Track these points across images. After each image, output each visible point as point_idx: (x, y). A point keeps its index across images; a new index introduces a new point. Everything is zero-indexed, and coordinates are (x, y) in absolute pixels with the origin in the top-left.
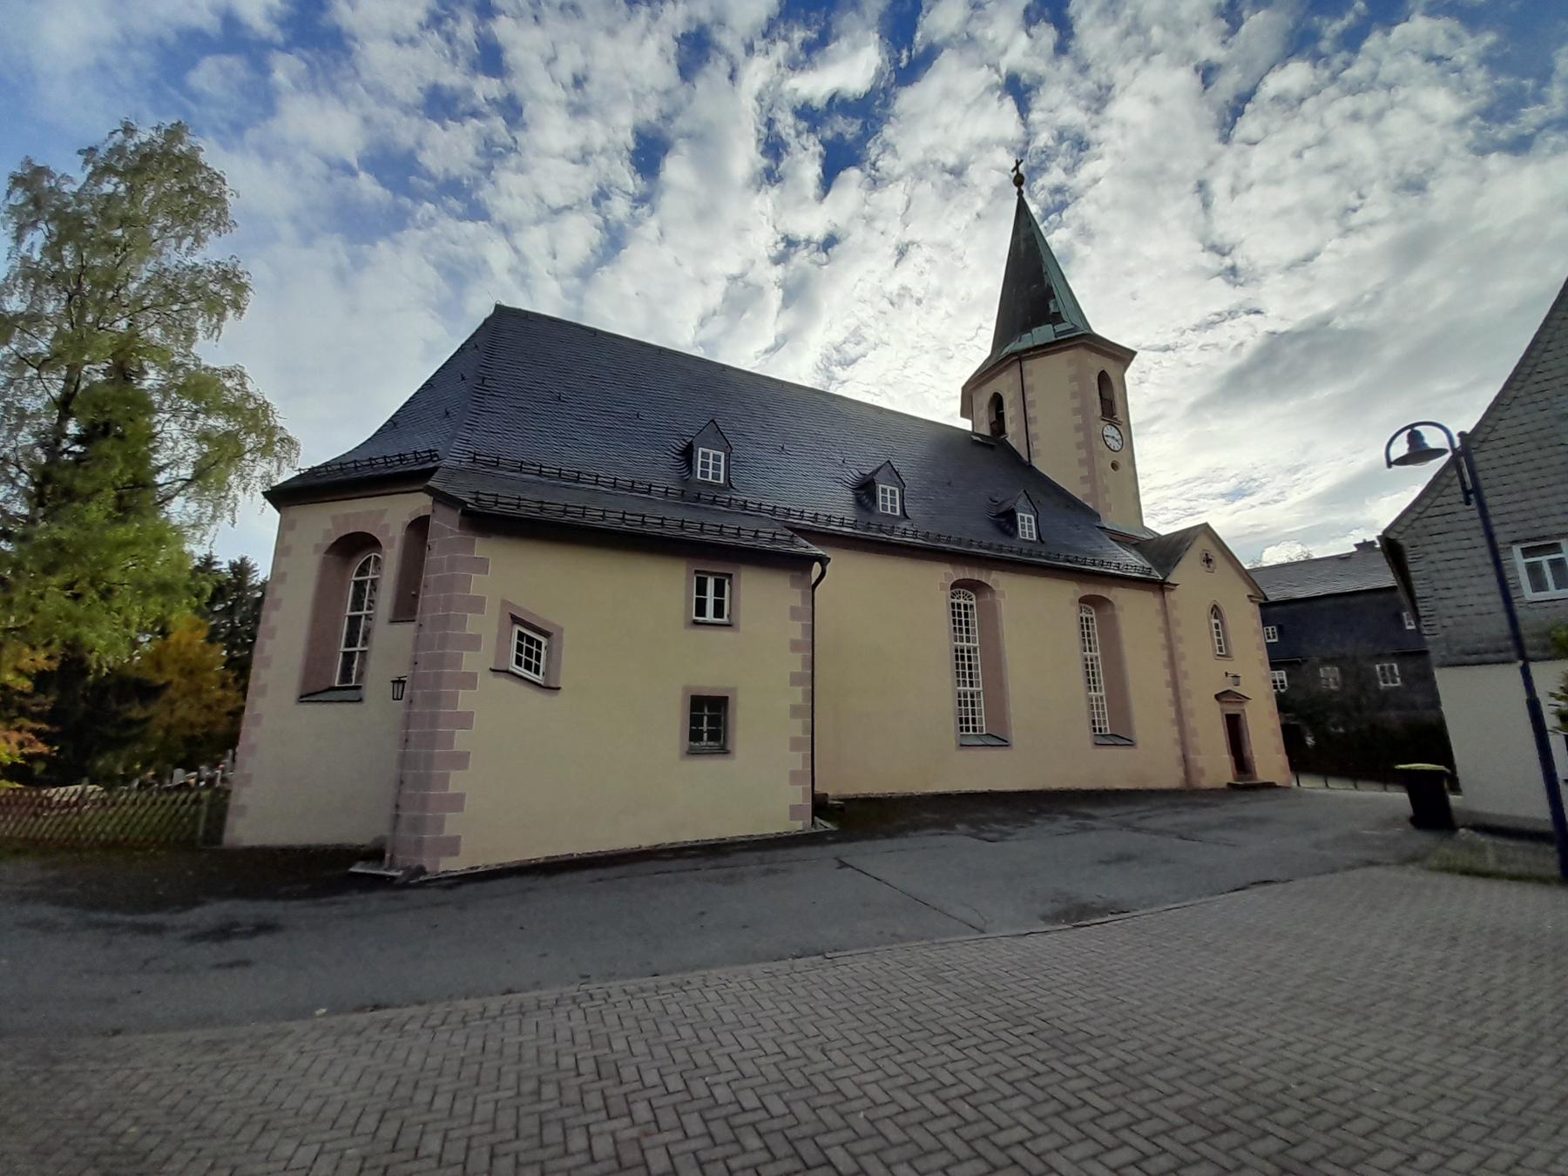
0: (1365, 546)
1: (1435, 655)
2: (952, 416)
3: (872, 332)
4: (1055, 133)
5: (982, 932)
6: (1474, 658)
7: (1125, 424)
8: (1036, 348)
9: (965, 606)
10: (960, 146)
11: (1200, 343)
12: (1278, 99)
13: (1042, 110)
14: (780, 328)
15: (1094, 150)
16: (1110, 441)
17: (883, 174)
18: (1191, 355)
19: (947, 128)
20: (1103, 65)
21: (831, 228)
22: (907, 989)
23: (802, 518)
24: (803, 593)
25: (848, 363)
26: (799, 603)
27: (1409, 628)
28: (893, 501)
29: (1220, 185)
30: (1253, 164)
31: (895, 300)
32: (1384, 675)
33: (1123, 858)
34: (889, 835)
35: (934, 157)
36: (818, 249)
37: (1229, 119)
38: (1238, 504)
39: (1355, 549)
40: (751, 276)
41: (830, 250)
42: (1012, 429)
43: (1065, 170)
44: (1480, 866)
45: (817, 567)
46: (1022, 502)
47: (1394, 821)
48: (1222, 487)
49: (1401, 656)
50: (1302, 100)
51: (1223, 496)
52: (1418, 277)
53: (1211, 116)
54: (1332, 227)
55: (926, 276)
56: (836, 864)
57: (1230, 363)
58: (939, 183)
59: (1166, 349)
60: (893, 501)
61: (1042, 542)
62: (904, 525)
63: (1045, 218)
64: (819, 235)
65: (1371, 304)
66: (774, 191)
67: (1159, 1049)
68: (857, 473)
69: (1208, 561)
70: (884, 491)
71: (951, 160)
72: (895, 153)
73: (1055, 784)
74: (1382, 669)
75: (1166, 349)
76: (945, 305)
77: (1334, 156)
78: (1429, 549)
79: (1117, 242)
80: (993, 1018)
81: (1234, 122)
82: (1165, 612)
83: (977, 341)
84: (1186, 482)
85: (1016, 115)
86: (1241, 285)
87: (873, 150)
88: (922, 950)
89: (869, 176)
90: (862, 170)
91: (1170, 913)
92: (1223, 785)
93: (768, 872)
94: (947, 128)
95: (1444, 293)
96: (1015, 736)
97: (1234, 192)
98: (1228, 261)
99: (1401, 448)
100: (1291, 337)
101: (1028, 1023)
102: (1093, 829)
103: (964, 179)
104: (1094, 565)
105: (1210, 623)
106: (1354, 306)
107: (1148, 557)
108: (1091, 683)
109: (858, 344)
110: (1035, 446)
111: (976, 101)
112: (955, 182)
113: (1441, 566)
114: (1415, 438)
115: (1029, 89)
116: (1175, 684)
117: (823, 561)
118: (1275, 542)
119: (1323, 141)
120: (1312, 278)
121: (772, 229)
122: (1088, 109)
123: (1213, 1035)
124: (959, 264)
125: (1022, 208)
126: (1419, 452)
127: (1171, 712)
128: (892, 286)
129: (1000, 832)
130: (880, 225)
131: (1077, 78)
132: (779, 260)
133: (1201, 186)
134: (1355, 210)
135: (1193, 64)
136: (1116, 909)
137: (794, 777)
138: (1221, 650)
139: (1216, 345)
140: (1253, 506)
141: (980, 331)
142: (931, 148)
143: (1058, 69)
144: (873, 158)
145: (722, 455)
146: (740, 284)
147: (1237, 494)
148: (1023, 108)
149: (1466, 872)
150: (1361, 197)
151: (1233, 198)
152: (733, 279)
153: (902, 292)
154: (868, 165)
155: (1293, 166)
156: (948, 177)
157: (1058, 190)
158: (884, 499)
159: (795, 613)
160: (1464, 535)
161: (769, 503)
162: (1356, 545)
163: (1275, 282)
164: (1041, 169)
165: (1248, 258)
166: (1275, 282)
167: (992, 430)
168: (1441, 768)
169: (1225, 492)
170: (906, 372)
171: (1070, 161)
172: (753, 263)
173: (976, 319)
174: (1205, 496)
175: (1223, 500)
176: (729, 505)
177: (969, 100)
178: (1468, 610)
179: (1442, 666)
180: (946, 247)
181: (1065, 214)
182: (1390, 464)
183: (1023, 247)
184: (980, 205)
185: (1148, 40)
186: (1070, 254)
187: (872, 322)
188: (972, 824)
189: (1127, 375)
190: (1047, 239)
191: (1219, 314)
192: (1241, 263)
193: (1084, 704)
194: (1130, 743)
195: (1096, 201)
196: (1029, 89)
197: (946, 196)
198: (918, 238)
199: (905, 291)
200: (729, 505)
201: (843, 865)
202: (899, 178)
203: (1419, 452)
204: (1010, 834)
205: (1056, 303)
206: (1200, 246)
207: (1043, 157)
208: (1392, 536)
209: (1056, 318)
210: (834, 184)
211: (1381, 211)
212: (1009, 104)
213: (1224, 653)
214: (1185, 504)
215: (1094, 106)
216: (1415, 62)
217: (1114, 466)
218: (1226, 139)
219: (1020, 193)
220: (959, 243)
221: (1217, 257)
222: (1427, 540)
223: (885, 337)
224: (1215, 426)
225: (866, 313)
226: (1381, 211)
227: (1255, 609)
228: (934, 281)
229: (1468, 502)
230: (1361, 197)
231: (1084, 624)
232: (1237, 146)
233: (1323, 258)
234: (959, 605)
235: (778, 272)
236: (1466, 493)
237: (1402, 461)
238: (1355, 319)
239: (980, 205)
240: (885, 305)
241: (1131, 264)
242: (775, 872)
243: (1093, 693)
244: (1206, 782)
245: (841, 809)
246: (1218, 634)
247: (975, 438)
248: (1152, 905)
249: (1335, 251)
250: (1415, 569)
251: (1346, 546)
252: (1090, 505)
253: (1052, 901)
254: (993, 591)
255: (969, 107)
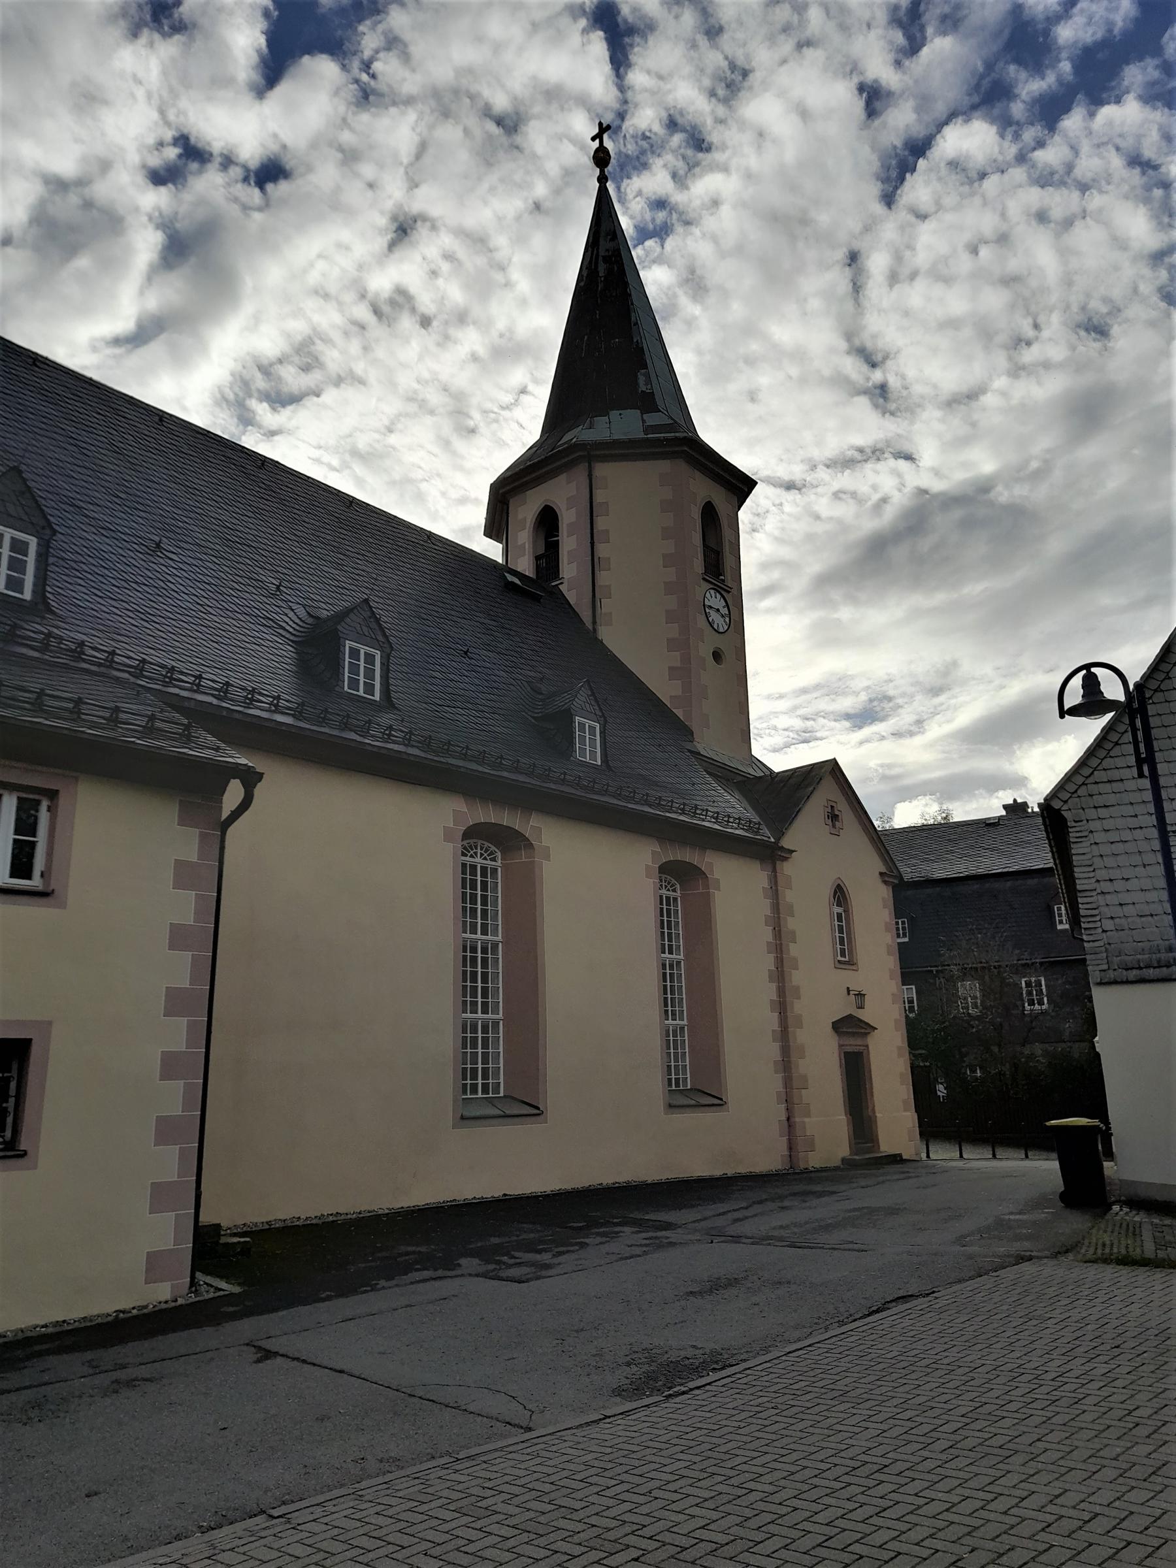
0: (1016, 809)
1: (1094, 973)
2: (466, 530)
3: (335, 354)
4: (664, 115)
5: (529, 1429)
6: (1133, 974)
7: (734, 591)
8: (615, 444)
9: (484, 870)
10: (518, 83)
11: (836, 486)
12: (955, 165)
13: (649, 72)
14: (152, 303)
15: (717, 156)
16: (714, 616)
17: (380, 85)
18: (823, 505)
19: (498, 48)
20: (740, 35)
21: (274, 147)
22: (430, 1535)
23: (197, 687)
24: (203, 837)
25: (281, 400)
26: (191, 854)
27: (1059, 927)
28: (370, 674)
29: (877, 263)
30: (919, 246)
31: (386, 309)
32: (1030, 993)
33: (716, 1286)
34: (347, 1289)
35: (475, 88)
36: (246, 180)
37: (894, 174)
38: (867, 731)
39: (1004, 813)
40: (102, 190)
41: (270, 187)
42: (570, 570)
43: (674, 176)
44: (1136, 1253)
45: (234, 793)
46: (582, 697)
47: (1039, 1203)
48: (847, 703)
49: (1049, 967)
50: (983, 176)
51: (848, 716)
52: (1091, 451)
53: (870, 160)
54: (1001, 360)
55: (440, 282)
56: (250, 1354)
57: (869, 525)
58: (478, 133)
59: (790, 486)
60: (370, 674)
61: (608, 767)
62: (386, 719)
63: (640, 241)
64: (251, 151)
65: (1038, 476)
66: (169, 48)
67: (807, 1543)
68: (301, 612)
69: (834, 817)
70: (355, 653)
71: (501, 102)
72: (406, 57)
73: (607, 1178)
74: (1028, 984)
75: (790, 486)
76: (471, 340)
77: (1014, 264)
78: (1093, 825)
79: (737, 310)
80: (577, 1550)
81: (902, 179)
82: (774, 891)
83: (518, 413)
84: (804, 691)
85: (607, 68)
86: (892, 414)
87: (369, 39)
88: (442, 1473)
89: (357, 81)
90: (344, 67)
91: (792, 1357)
92: (838, 1163)
93: (118, 1386)
94: (498, 48)
95: (1115, 480)
96: (555, 1096)
97: (893, 278)
98: (877, 376)
99: (1075, 695)
100: (949, 501)
101: (628, 1546)
102: (672, 1244)
103: (518, 139)
104: (683, 812)
105: (831, 913)
106: (1016, 474)
107: (755, 805)
108: (668, 1005)
109: (306, 369)
110: (607, 606)
111: (550, 21)
112: (504, 140)
113: (1105, 849)
114: (1091, 684)
115: (631, 31)
116: (782, 1006)
117: (250, 779)
118: (909, 793)
119: (1003, 239)
120: (974, 425)
121: (155, 115)
122: (712, 94)
123: (868, 1511)
124: (499, 277)
125: (604, 213)
126: (1093, 703)
127: (773, 1050)
128: (381, 282)
129: (533, 1264)
130: (368, 170)
131: (703, 41)
132: (158, 178)
133: (853, 258)
134: (1029, 343)
135: (856, 80)
136: (716, 1362)
137: (160, 1196)
138: (843, 955)
139: (854, 495)
140: (883, 738)
141: (525, 399)
142: (469, 71)
143: (677, 17)
144: (367, 54)
145: (33, 542)
146: (74, 199)
147: (863, 717)
148: (619, 60)
149: (1125, 1261)
150: (1036, 326)
151: (891, 286)
152: (58, 185)
153: (400, 299)
154: (356, 64)
155: (965, 263)
156: (492, 127)
157: (660, 204)
158: (354, 669)
159: (184, 875)
160: (1130, 810)
161: (129, 653)
162: (1005, 807)
163: (931, 415)
164: (638, 164)
165: (903, 377)
166: (931, 415)
167: (538, 568)
168: (1096, 1122)
169: (851, 711)
170: (393, 439)
171: (681, 165)
172: (105, 166)
173: (518, 375)
174: (826, 715)
175: (847, 724)
176: (45, 647)
177: (538, 15)
178: (1129, 910)
179: (1100, 984)
180: (478, 241)
181: (670, 243)
182: (1062, 714)
183: (602, 269)
184: (541, 190)
185: (803, 23)
186: (672, 309)
187: (336, 336)
188: (484, 1255)
189: (741, 514)
190: (642, 274)
191: (861, 450)
192: (893, 382)
193: (657, 1041)
194: (718, 1103)
195: (715, 239)
196: (631, 31)
197: (487, 157)
198: (435, 211)
199: (402, 299)
200: (45, 647)
201: (268, 1355)
202: (409, 101)
203: (1093, 703)
204: (548, 1267)
205: (648, 376)
206: (843, 345)
207: (644, 144)
208: (1056, 804)
209: (648, 403)
210: (292, 70)
211: (1057, 353)
212: (598, 45)
213: (846, 958)
214: (798, 724)
215: (721, 92)
216: (1117, 162)
217: (717, 656)
218: (889, 200)
219: (602, 179)
220: (501, 241)
221: (865, 368)
222: (1092, 814)
223: (359, 368)
224: (845, 613)
225: (328, 318)
226: (1057, 353)
227: (885, 892)
228: (456, 294)
229: (1141, 775)
230: (1036, 326)
231: (665, 908)
232: (901, 214)
233: (989, 400)
234: (473, 868)
235: (155, 199)
236: (1140, 762)
237: (1075, 711)
238: (1020, 492)
239: (541, 190)
240: (363, 313)
241: (754, 347)
242: (131, 1383)
243: (670, 1022)
244: (814, 1160)
245: (245, 1250)
246: (841, 931)
247: (510, 578)
248: (766, 1350)
249: (1004, 394)
250: (1080, 851)
251: (992, 806)
252: (679, 713)
253: (628, 1364)
254: (529, 845)
255: (535, 27)
